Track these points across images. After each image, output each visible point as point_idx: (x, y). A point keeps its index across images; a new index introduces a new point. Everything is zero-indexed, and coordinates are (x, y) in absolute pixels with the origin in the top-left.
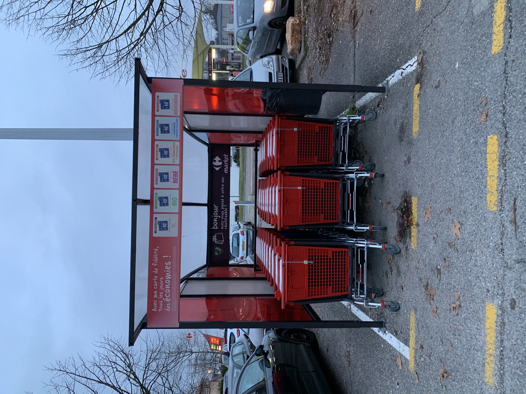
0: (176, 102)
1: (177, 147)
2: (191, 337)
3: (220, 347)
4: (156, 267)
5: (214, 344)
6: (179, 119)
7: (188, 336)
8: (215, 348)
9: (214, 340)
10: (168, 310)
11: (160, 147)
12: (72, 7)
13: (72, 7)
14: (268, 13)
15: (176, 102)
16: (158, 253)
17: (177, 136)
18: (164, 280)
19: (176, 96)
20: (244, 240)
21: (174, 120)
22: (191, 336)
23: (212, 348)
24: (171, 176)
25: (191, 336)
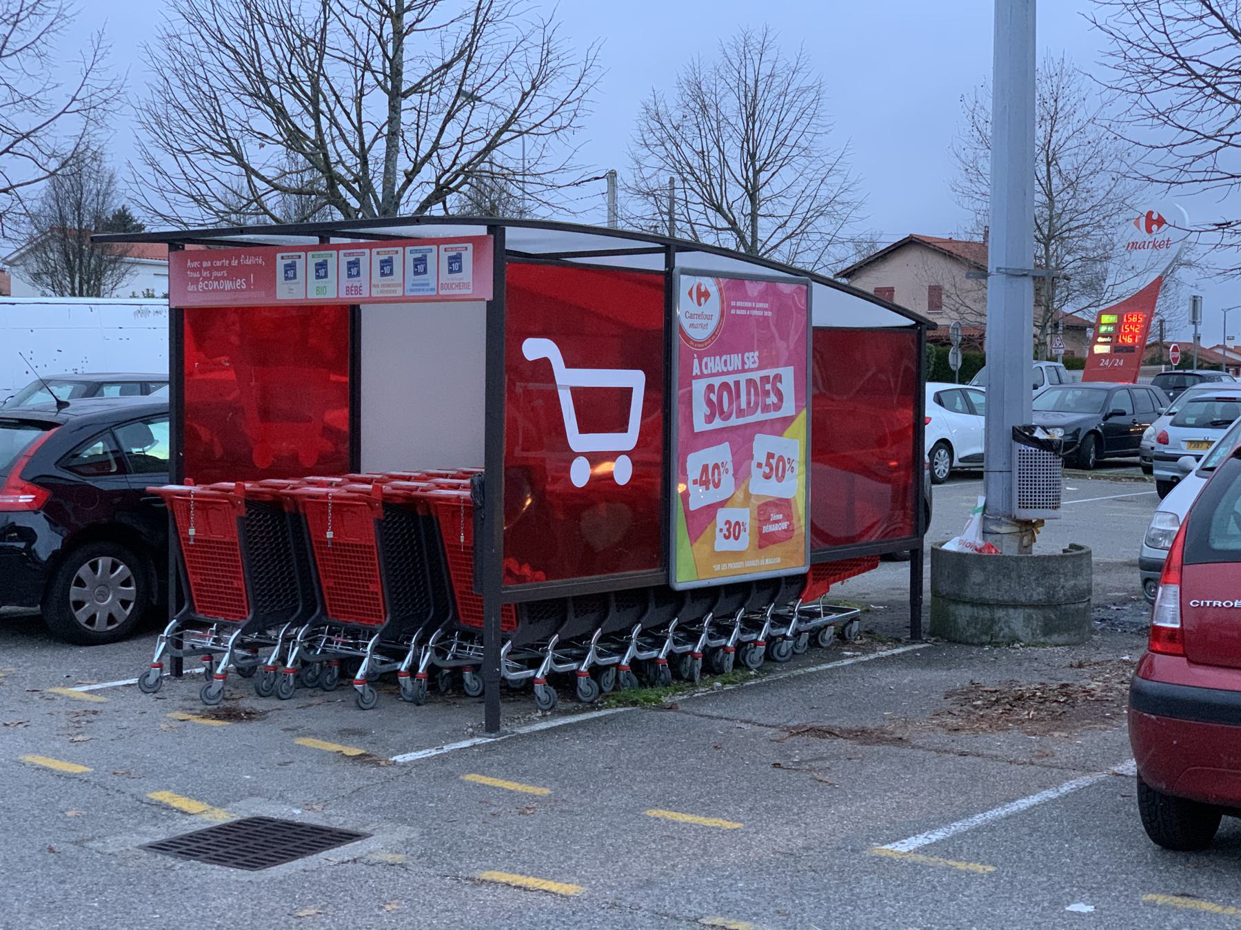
0: (458, 286)
1: (396, 291)
2: (1149, 231)
3: (1105, 349)
4: (239, 262)
5: (1117, 326)
6: (434, 293)
7: (1155, 217)
8: (1103, 329)
9: (1135, 324)
10: (191, 288)
11: (395, 257)
12: (254, 40)
13: (254, 40)
14: (583, 488)
15: (458, 286)
16: (257, 265)
17: (411, 290)
18: (224, 278)
19: (466, 286)
20: (112, 392)
21: (433, 284)
22: (1154, 227)
23: (1106, 319)
24: (355, 282)
25: (1154, 227)
